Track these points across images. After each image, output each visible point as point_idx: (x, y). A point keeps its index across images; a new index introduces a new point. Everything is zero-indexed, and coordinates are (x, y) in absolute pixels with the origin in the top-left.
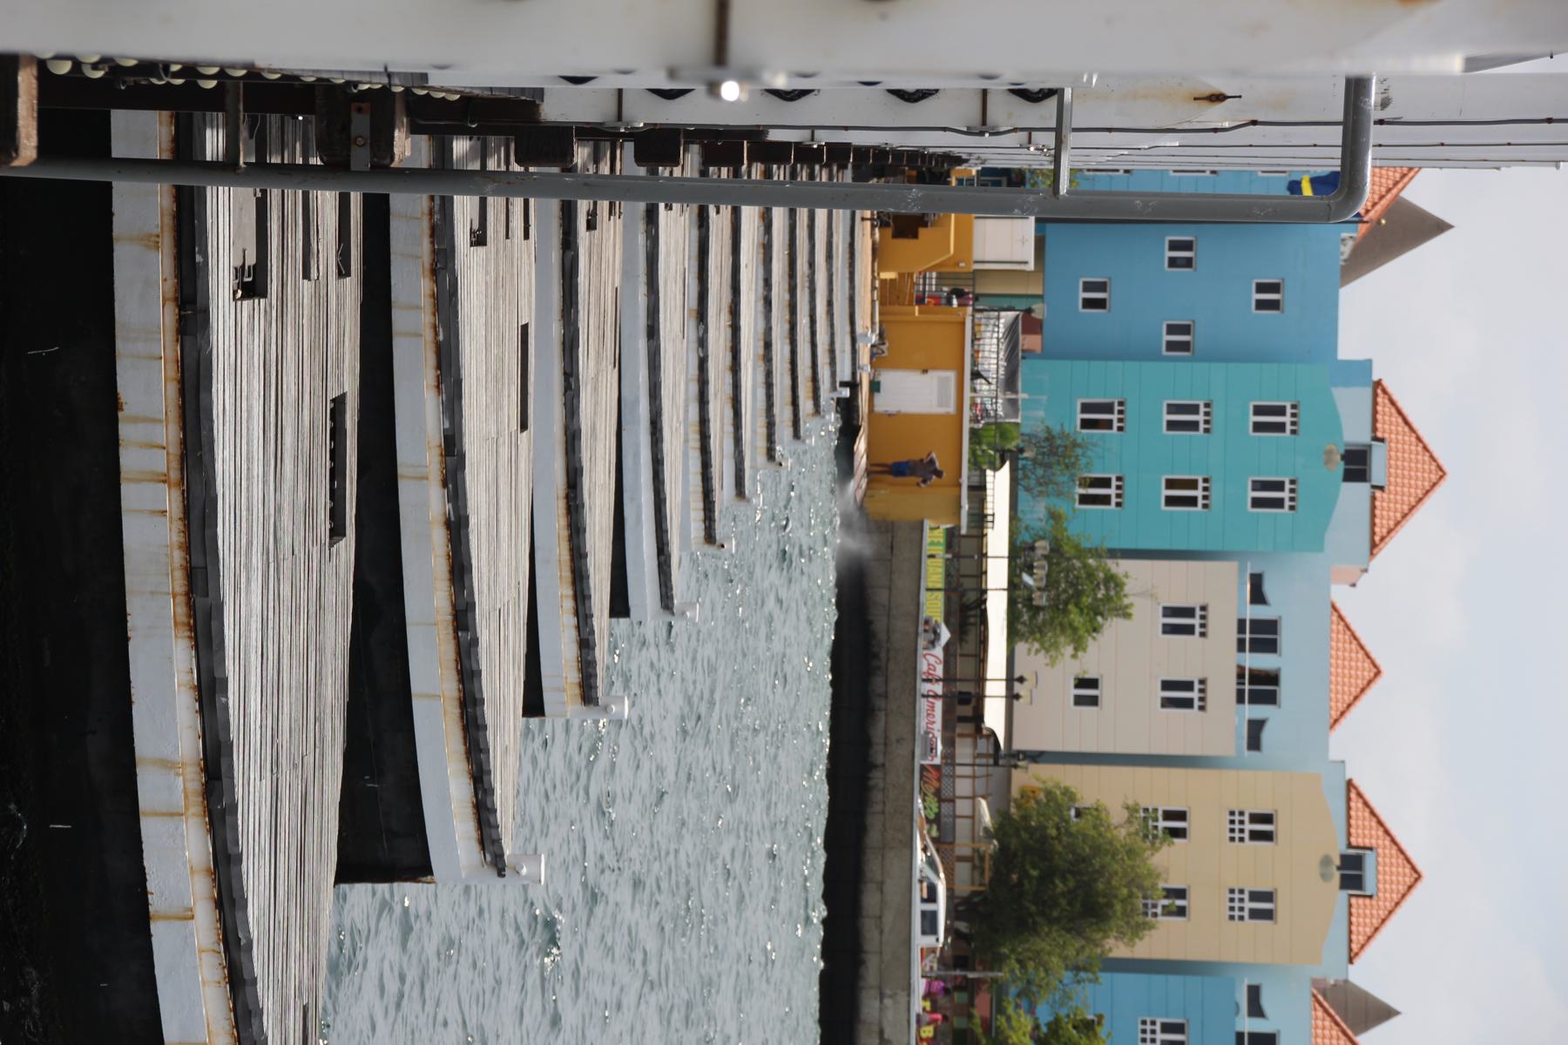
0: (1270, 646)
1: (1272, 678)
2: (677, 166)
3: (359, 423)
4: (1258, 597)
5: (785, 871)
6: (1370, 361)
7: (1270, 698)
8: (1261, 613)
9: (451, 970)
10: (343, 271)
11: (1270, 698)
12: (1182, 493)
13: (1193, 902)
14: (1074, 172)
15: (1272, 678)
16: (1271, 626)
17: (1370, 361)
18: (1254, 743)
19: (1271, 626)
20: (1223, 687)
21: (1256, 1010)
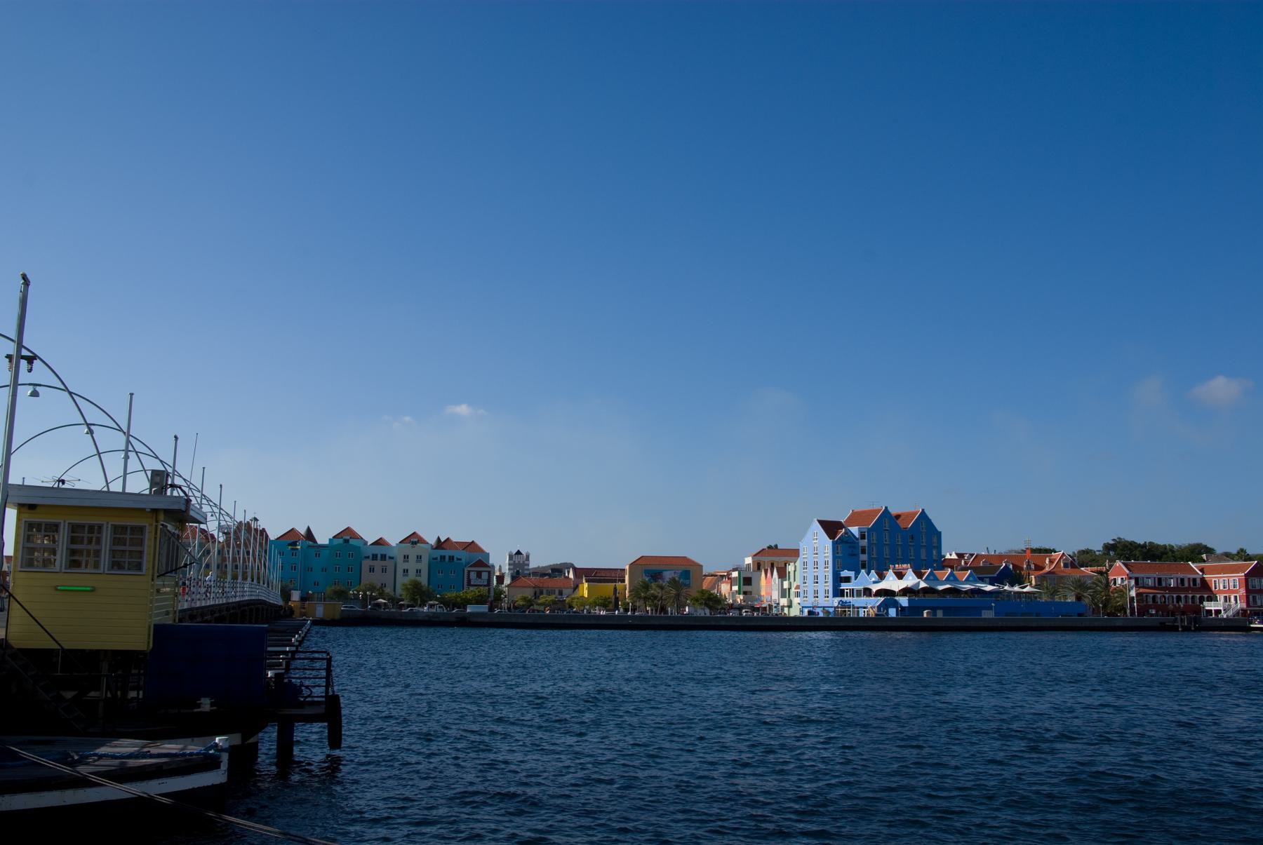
0: (376, 555)
1: (382, 555)
2: (786, 580)
3: (158, 778)
4: (368, 557)
5: (394, 697)
6: (751, 585)
7: (385, 555)
8: (371, 557)
9: (689, 688)
10: (789, 572)
11: (385, 555)
12: (384, 570)
13: (406, 568)
14: (21, 567)
15: (382, 555)
16: (373, 555)
17: (751, 585)
18: (392, 558)
19: (373, 555)
20: (383, 563)
21: (436, 559)
